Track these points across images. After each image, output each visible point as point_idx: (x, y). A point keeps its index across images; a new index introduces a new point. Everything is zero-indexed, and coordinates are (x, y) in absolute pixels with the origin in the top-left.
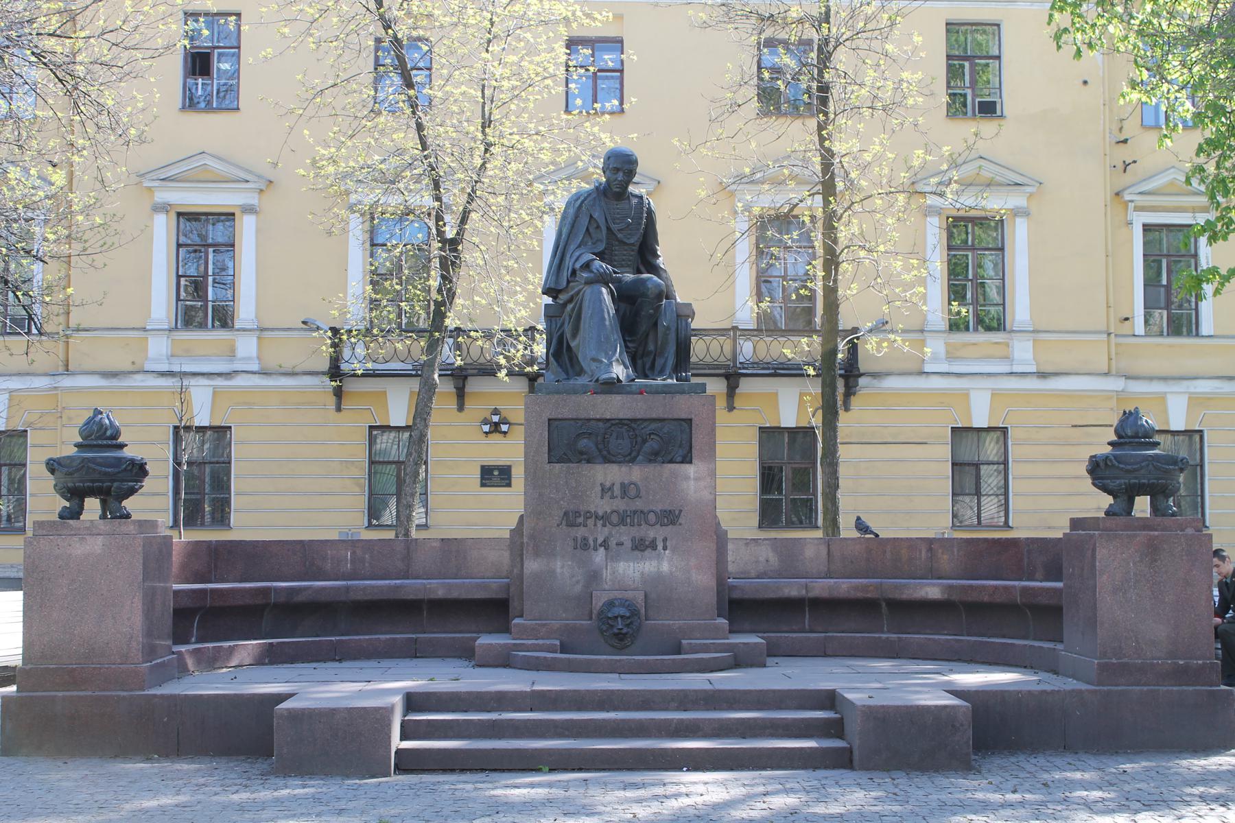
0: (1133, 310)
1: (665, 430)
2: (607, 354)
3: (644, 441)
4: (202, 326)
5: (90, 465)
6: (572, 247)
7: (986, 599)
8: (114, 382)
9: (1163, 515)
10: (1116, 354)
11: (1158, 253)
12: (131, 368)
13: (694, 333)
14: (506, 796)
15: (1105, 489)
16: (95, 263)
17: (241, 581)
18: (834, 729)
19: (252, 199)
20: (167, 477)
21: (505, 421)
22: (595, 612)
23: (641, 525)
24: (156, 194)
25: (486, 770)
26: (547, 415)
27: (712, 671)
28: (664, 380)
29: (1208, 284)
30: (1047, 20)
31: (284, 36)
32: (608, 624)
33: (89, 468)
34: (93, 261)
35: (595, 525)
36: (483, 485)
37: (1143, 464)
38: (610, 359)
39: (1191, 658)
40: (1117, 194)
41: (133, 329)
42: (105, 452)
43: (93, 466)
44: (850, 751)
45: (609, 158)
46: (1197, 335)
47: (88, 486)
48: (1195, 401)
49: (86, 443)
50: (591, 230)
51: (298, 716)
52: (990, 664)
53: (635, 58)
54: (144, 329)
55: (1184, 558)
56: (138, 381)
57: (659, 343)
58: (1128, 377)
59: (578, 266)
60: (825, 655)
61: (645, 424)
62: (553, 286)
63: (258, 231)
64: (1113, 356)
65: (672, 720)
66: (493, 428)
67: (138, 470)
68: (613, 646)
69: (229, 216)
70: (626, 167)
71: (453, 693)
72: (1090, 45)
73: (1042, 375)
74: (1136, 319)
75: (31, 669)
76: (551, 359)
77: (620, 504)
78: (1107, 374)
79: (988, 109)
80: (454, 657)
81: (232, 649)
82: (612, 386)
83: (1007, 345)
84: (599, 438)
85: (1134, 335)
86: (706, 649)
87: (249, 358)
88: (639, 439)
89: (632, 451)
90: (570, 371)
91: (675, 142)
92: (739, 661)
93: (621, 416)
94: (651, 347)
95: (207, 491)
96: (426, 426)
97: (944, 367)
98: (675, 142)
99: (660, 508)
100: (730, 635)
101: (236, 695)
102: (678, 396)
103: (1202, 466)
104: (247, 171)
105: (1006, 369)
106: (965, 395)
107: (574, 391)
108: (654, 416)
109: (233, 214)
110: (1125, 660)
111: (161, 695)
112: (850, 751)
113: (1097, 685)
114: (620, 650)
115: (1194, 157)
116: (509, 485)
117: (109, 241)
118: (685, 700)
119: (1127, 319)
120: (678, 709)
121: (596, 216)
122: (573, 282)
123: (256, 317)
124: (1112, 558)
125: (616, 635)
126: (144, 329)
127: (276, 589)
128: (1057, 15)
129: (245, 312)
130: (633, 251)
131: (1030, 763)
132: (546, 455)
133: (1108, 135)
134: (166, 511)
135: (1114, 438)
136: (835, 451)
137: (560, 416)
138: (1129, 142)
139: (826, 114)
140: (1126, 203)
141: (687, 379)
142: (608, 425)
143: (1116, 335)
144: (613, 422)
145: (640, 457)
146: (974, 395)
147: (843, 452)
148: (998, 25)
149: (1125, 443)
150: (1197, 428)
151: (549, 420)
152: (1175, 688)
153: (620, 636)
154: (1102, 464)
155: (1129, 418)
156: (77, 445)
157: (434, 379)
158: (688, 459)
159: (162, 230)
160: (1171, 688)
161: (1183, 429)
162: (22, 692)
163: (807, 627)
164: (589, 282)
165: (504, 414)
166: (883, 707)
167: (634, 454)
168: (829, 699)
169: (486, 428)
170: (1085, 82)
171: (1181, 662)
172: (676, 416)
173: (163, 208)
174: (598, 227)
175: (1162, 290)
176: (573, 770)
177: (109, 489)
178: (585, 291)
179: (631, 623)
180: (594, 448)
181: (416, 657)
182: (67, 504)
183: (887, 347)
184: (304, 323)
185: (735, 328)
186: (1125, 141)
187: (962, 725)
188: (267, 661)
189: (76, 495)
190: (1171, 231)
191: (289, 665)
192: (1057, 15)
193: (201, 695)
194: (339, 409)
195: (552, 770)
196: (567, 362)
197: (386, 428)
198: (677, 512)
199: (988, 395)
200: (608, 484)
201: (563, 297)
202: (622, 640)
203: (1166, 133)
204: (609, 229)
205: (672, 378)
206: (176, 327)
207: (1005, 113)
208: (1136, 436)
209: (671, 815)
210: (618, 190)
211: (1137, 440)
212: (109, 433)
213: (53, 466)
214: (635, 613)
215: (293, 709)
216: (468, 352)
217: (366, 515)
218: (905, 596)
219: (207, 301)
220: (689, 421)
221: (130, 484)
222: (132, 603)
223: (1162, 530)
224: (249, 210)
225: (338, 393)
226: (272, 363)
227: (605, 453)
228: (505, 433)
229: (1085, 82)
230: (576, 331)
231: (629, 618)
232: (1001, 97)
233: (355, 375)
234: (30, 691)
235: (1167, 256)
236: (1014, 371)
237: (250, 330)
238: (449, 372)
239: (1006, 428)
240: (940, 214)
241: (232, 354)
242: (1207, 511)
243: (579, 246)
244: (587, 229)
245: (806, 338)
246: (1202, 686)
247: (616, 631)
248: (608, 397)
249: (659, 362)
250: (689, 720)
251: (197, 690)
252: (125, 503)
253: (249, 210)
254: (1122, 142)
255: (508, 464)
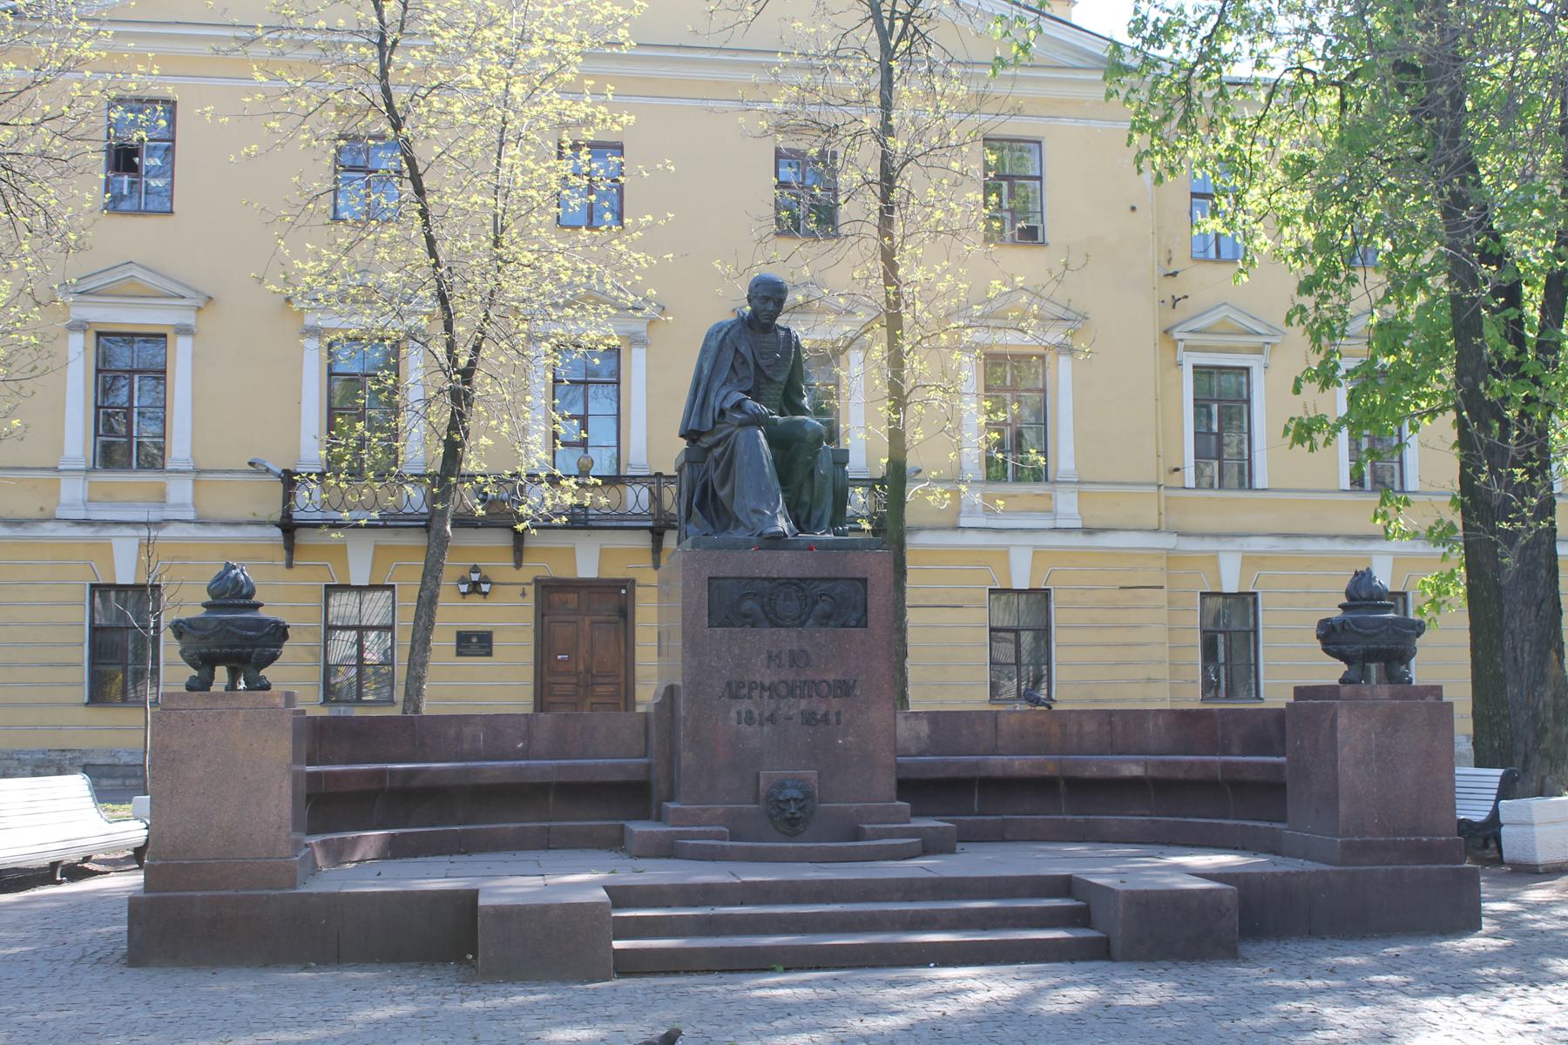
0: (1183, 461)
1: (838, 590)
2: (769, 505)
3: (815, 603)
4: (127, 466)
5: (229, 627)
6: (716, 385)
7: (1181, 775)
8: (19, 532)
9: (1400, 683)
10: (1166, 508)
11: (1208, 397)
12: (39, 515)
13: (852, 483)
14: (774, 996)
15: (1340, 655)
16: (23, 391)
17: (347, 763)
18: (1077, 918)
19: (189, 318)
20: (82, 644)
21: (486, 580)
22: (762, 794)
23: (811, 697)
24: (72, 310)
25: (714, 971)
26: (706, 573)
27: (905, 859)
28: (823, 534)
29: (1319, 433)
30: (1126, 141)
31: (273, 131)
32: (779, 807)
33: (228, 631)
34: (21, 388)
35: (761, 697)
36: (459, 654)
37: (1383, 628)
38: (773, 510)
39: (1433, 835)
40: (1166, 332)
41: (42, 469)
42: (243, 613)
43: (232, 629)
44: (1107, 941)
45: (757, 285)
46: (1250, 488)
47: (214, 652)
48: (1250, 560)
49: (218, 602)
50: (736, 366)
51: (505, 914)
52: (1193, 846)
53: (673, 168)
54: (56, 469)
55: (1426, 728)
56: (47, 530)
57: (816, 494)
58: (1180, 534)
59: (727, 405)
60: (1003, 840)
61: (816, 583)
62: (696, 428)
63: (195, 355)
64: (1163, 511)
65: (907, 911)
66: (471, 589)
67: (279, 632)
68: (784, 833)
69: (158, 338)
70: (777, 296)
71: (654, 886)
72: (1172, 170)
73: (1089, 531)
74: (1186, 470)
75: (161, 865)
76: (695, 510)
77: (788, 675)
78: (1157, 531)
79: (1030, 235)
80: (592, 848)
81: (356, 840)
82: (777, 541)
83: (1050, 497)
84: (765, 600)
85: (1185, 488)
86: (891, 834)
87: (183, 505)
88: (810, 600)
89: (801, 614)
90: (717, 525)
91: (717, 264)
92: (930, 846)
93: (789, 574)
94: (806, 498)
95: (129, 662)
96: (438, 585)
97: (981, 522)
98: (717, 264)
99: (833, 677)
100: (912, 819)
101: (405, 892)
102: (851, 553)
103: (1256, 632)
104: (187, 287)
105: (1049, 524)
106: (1004, 553)
107: (735, 546)
108: (826, 575)
109: (165, 336)
110: (1368, 838)
111: (319, 893)
112: (1107, 941)
113: (1341, 865)
114: (792, 836)
115: (1296, 296)
116: (489, 654)
117: (42, 365)
118: (868, 890)
119: (1177, 470)
120: (903, 899)
121: (742, 350)
122: (720, 423)
123: (192, 457)
124: (1354, 729)
125: (788, 820)
126: (56, 469)
127: (392, 771)
128: (1136, 136)
129: (179, 449)
130: (780, 389)
131: (1292, 948)
132: (706, 618)
133: (1156, 267)
134: (81, 684)
135: (1344, 600)
136: (904, 615)
137: (721, 575)
138: (1178, 275)
139: (891, 237)
140: (1176, 342)
141: (844, 533)
142: (774, 584)
143: (1166, 488)
144: (781, 581)
145: (811, 621)
146: (1013, 552)
147: (912, 616)
148: (1040, 143)
149: (1361, 606)
150: (1251, 590)
151: (710, 578)
152: (1421, 867)
153: (793, 822)
154: (1338, 629)
155: (1363, 578)
156: (205, 605)
157: (446, 531)
158: (863, 622)
159: (78, 357)
160: (1415, 867)
161: (1236, 591)
162: (149, 892)
163: (976, 809)
164: (742, 425)
165: (485, 572)
166: (1146, 891)
167: (804, 617)
168: (1065, 886)
169: (464, 588)
170: (1133, 209)
171: (1425, 839)
172: (849, 576)
173: (81, 326)
174: (745, 362)
175: (1213, 438)
176: (810, 969)
177: (249, 655)
178: (737, 435)
179: (804, 806)
180: (759, 610)
181: (549, 848)
182: (195, 673)
183: (950, 499)
184: (251, 464)
185: (659, 475)
186: (1174, 274)
187: (1228, 910)
188: (389, 855)
189: (204, 662)
190: (1223, 374)
191: (414, 860)
192: (1136, 136)
193: (366, 893)
194: (290, 565)
195: (787, 970)
196: (713, 513)
197: (346, 588)
198: (852, 682)
199: (1030, 552)
200: (775, 651)
201: (706, 441)
202: (793, 825)
203: (1241, 267)
204: (756, 364)
205: (830, 533)
206: (94, 468)
207: (1048, 240)
208: (1370, 598)
209: (980, 1011)
210: (766, 321)
211: (1373, 603)
212: (244, 591)
213: (180, 629)
214: (809, 795)
215: (500, 906)
216: (409, 500)
217: (322, 689)
218: (1088, 773)
219: (132, 437)
220: (864, 581)
221: (273, 650)
222: (280, 787)
223: (1403, 699)
224: (184, 330)
225: (290, 546)
226: (212, 510)
227: (771, 616)
228: (485, 594)
229: (1133, 209)
230: (725, 478)
231: (802, 801)
232: (1042, 222)
233: (358, 526)
234: (159, 891)
235: (1218, 401)
236: (1058, 526)
237: (184, 472)
238: (423, 523)
239: (1049, 590)
240: (85, 330)
241: (161, 499)
242: (1262, 682)
243: (724, 384)
244: (733, 365)
245: (860, 489)
246: (1446, 863)
247: (788, 815)
248: (775, 553)
249: (816, 514)
250: (925, 911)
251: (356, 887)
252: (262, 673)
253: (184, 330)
254: (1170, 274)
255: (489, 629)
